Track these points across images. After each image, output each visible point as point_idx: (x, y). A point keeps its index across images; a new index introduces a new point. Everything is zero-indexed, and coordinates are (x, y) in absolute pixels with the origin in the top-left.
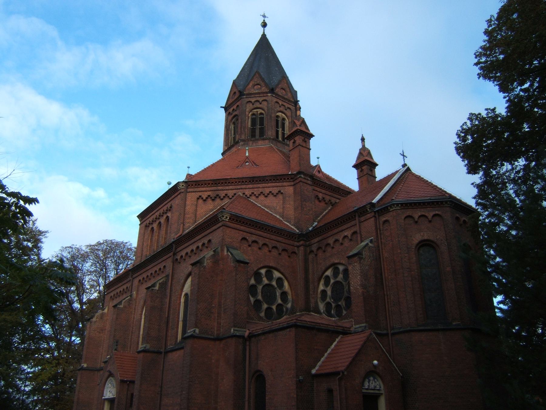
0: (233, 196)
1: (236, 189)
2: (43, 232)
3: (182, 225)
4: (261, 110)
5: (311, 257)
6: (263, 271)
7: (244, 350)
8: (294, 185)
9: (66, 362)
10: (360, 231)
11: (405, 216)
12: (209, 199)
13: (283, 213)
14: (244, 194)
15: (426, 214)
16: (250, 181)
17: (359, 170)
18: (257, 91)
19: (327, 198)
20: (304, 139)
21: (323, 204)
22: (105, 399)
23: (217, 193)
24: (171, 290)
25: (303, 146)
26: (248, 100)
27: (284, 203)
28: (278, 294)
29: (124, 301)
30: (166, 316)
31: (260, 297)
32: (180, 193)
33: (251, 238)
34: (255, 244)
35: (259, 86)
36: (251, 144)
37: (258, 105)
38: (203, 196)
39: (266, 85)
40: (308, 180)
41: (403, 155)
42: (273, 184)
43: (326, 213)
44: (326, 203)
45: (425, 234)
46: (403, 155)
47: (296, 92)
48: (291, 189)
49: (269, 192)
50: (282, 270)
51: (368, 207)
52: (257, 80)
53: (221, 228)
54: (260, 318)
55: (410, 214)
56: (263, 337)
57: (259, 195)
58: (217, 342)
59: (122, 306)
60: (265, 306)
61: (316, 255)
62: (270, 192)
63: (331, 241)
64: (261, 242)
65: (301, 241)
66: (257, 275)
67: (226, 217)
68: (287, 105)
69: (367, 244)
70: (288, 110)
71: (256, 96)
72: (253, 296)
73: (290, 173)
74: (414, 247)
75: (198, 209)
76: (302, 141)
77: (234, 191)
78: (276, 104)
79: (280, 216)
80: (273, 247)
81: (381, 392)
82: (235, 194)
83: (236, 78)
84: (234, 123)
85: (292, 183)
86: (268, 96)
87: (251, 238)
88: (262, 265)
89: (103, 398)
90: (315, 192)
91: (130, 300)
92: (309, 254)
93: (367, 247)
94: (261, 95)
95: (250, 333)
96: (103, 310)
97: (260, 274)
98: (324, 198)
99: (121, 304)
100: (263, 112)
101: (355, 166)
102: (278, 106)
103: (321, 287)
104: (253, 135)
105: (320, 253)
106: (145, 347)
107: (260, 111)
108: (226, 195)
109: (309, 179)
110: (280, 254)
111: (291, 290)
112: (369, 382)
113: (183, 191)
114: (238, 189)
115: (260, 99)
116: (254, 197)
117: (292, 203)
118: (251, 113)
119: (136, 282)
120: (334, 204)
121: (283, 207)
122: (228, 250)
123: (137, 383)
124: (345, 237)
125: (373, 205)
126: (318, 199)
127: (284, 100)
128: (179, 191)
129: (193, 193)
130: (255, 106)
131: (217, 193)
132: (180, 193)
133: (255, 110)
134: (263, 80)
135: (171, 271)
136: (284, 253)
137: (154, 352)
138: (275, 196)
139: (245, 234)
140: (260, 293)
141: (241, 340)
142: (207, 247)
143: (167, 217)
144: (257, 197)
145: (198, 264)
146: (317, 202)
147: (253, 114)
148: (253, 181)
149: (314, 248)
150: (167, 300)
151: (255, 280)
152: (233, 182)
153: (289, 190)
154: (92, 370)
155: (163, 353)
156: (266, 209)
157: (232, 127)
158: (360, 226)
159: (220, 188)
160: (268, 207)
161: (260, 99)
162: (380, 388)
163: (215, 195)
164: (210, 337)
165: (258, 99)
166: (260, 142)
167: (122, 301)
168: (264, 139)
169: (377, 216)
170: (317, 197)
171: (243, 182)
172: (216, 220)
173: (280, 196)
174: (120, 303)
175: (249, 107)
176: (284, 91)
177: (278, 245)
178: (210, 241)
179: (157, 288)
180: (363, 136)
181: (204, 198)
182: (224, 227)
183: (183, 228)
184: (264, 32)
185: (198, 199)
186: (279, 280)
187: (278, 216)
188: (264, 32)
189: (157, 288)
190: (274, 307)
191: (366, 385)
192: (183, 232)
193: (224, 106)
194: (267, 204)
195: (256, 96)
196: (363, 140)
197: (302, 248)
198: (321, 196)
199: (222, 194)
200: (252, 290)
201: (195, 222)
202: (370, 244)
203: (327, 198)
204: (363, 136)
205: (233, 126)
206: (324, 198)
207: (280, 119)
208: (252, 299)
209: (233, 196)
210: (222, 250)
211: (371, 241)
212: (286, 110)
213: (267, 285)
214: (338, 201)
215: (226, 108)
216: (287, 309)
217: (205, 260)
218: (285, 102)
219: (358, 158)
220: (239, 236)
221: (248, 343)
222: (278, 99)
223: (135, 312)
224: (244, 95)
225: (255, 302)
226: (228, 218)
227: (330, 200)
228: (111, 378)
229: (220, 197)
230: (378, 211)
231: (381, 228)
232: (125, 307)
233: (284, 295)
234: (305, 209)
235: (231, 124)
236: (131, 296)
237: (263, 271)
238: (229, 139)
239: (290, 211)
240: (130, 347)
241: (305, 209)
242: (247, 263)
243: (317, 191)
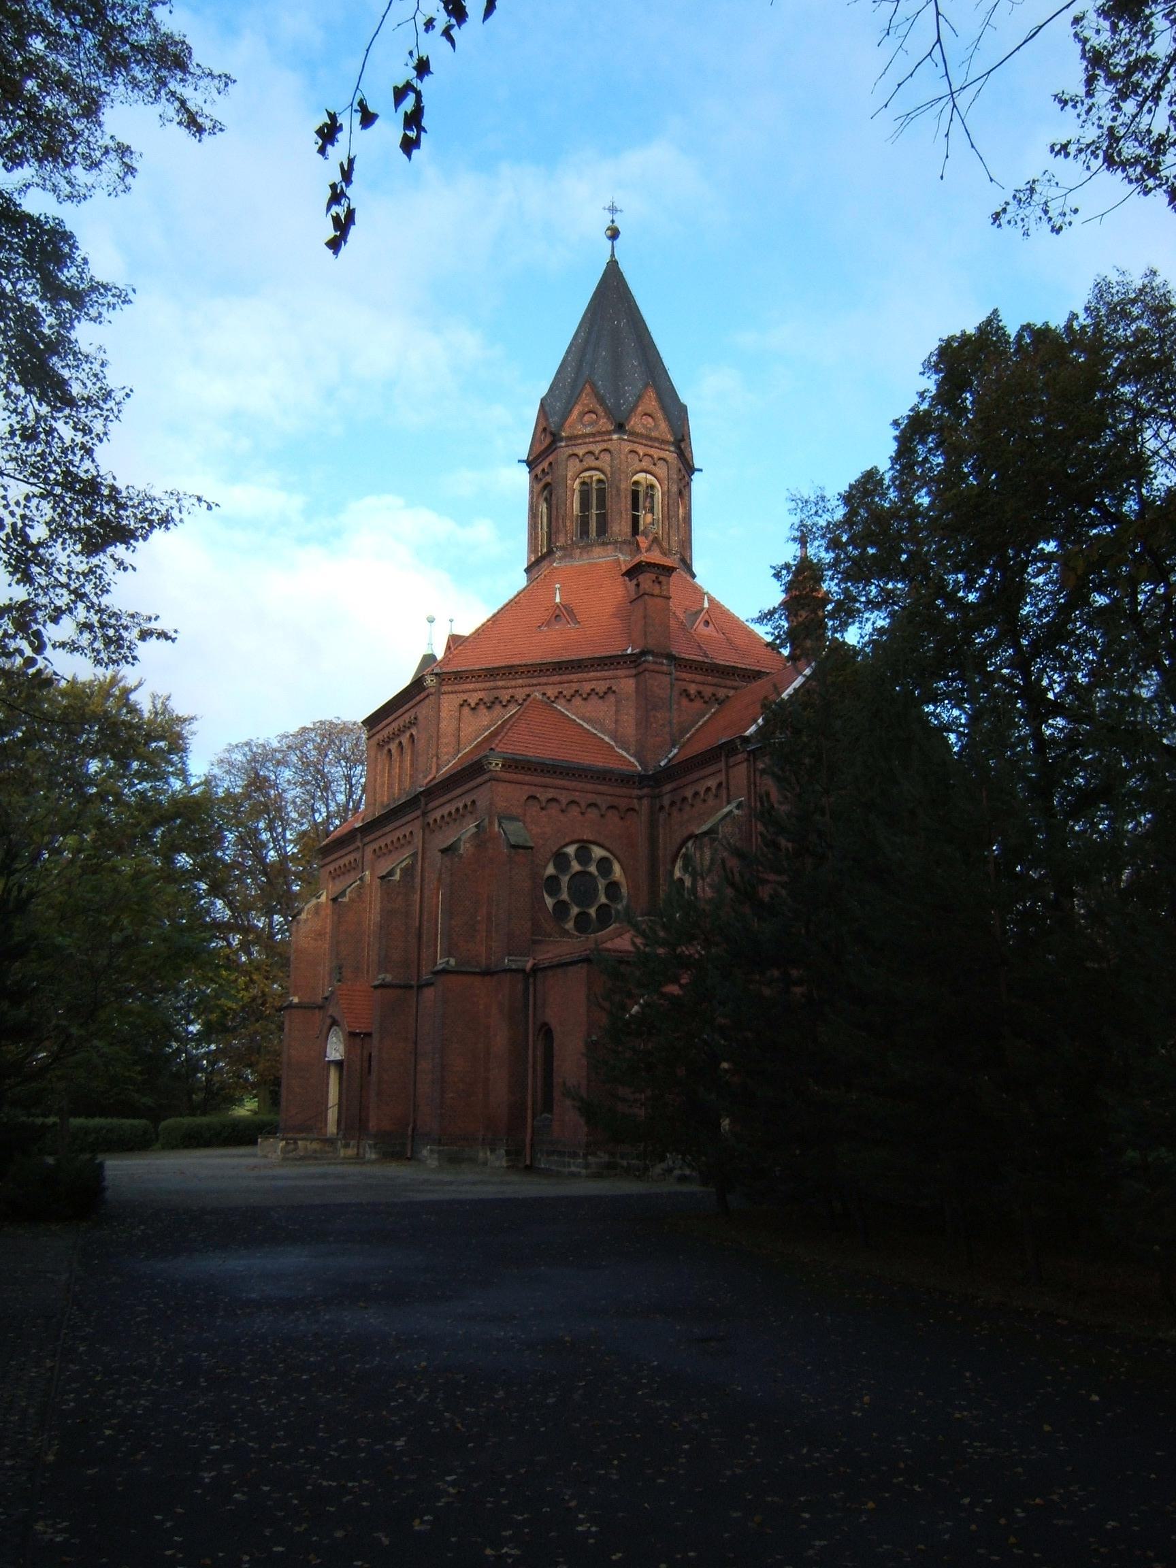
0: (524, 700)
1: (529, 686)
2: (185, 720)
3: (434, 760)
4: (597, 473)
5: (662, 816)
6: (571, 850)
7: (526, 989)
8: (635, 676)
9: (267, 978)
10: (728, 783)
12: (482, 706)
13: (616, 732)
14: (544, 694)
16: (554, 669)
18: (588, 430)
19: (708, 691)
21: (698, 704)
22: (329, 1061)
23: (496, 693)
24: (422, 880)
25: (652, 595)
26: (571, 452)
27: (617, 711)
28: (600, 887)
29: (349, 890)
30: (417, 924)
31: (565, 896)
32: (428, 696)
33: (544, 795)
34: (554, 804)
35: (594, 416)
36: (577, 556)
37: (590, 462)
38: (470, 701)
39: (609, 413)
40: (662, 664)
42: (598, 674)
43: (705, 723)
44: (705, 702)
47: (683, 409)
48: (632, 682)
50: (607, 845)
51: (738, 742)
52: (587, 400)
53: (489, 784)
54: (566, 933)
56: (550, 973)
57: (572, 696)
58: (487, 978)
59: (346, 899)
60: (575, 910)
61: (669, 814)
62: (593, 690)
63: (689, 793)
64: (564, 798)
65: (643, 787)
66: (561, 860)
67: (496, 764)
68: (656, 453)
69: (731, 812)
70: (661, 463)
71: (587, 440)
72: (551, 895)
73: (629, 651)
75: (462, 725)
76: (651, 584)
77: (527, 690)
78: (632, 455)
79: (611, 738)
80: (590, 805)
82: (528, 696)
83: (546, 391)
84: (546, 499)
85: (633, 672)
86: (611, 440)
87: (544, 795)
88: (567, 840)
90: (680, 683)
91: (360, 887)
93: (728, 819)
94: (597, 439)
95: (534, 965)
96: (319, 897)
97: (566, 855)
98: (699, 693)
99: (345, 896)
100: (602, 477)
102: (637, 458)
104: (585, 532)
105: (675, 813)
106: (383, 980)
107: (597, 475)
108: (512, 697)
110: (602, 816)
111: (626, 877)
113: (433, 690)
114: (533, 685)
115: (597, 448)
116: (562, 701)
117: (632, 711)
118: (578, 481)
119: (369, 851)
120: (723, 701)
121: (617, 721)
122: (500, 825)
123: (376, 1036)
124: (708, 789)
125: (746, 740)
126: (688, 695)
127: (650, 443)
128: (427, 691)
129: (451, 696)
130: (585, 464)
131: (496, 693)
132: (428, 696)
133: (587, 474)
134: (601, 400)
135: (420, 844)
136: (610, 813)
137: (400, 987)
138: (602, 698)
139: (534, 788)
140: (566, 890)
141: (520, 976)
142: (471, 813)
143: (412, 735)
144: (569, 700)
145: (450, 852)
146: (685, 701)
147: (583, 483)
148: (560, 669)
149: (666, 801)
150: (417, 897)
151: (556, 866)
152: (522, 672)
153: (627, 685)
154: (308, 1008)
155: (415, 988)
156: (585, 725)
157: (543, 507)
158: (727, 774)
159: (500, 683)
160: (588, 721)
161: (597, 448)
163: (492, 699)
164: (473, 970)
165: (592, 447)
166: (597, 551)
167: (345, 890)
168: (604, 544)
169: (751, 759)
170: (685, 693)
171: (541, 671)
173: (611, 698)
174: (343, 894)
175: (573, 466)
176: (650, 420)
177: (599, 800)
178: (473, 802)
179: (397, 877)
181: (473, 705)
182: (494, 782)
183: (438, 765)
184: (613, 255)
185: (461, 705)
186: (604, 865)
187: (607, 739)
188: (613, 255)
189: (397, 877)
190: (592, 911)
192: (437, 772)
194: (587, 714)
195: (587, 440)
197: (645, 802)
198: (692, 689)
199: (505, 697)
200: (552, 885)
201: (459, 751)
202: (736, 812)
203: (708, 691)
205: (545, 505)
206: (699, 693)
207: (641, 489)
208: (549, 902)
209: (524, 700)
210: (491, 823)
211: (739, 807)
212: (655, 464)
213: (578, 873)
214: (731, 693)
215: (531, 463)
216: (618, 912)
217: (462, 843)
218: (651, 447)
220: (522, 793)
221: (531, 980)
222: (635, 442)
223: (371, 908)
224: (561, 440)
225: (555, 905)
227: (714, 695)
228: (335, 1027)
229: (501, 702)
230: (753, 751)
231: (758, 781)
232: (352, 900)
233: (613, 888)
234: (654, 725)
235: (541, 501)
236: (361, 879)
237: (571, 850)
238: (536, 538)
239: (629, 729)
240: (368, 971)
241: (654, 725)
242: (531, 848)
243: (685, 680)
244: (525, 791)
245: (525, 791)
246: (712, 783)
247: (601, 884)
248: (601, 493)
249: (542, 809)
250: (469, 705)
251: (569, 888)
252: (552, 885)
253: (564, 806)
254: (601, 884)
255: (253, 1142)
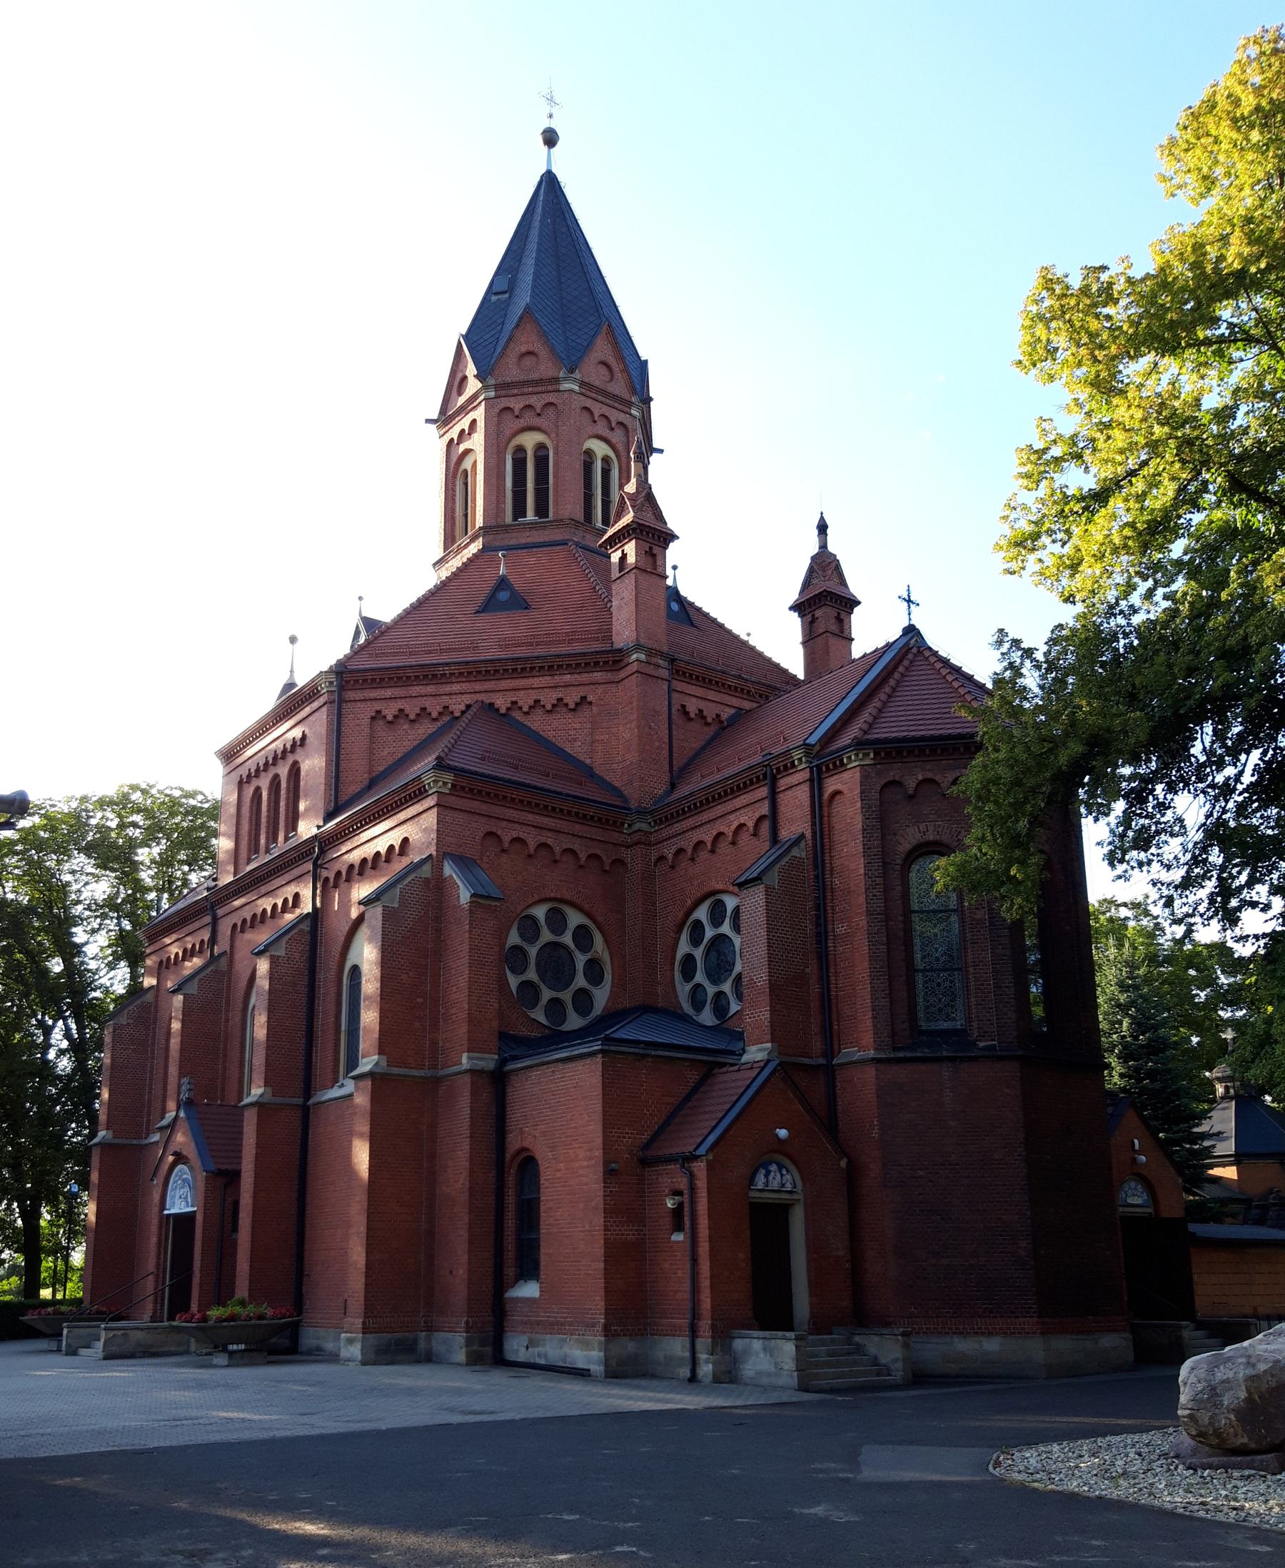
0: (463, 712)
6: (540, 912)
11: (883, 781)
15: (938, 778)
17: (806, 618)
20: (651, 548)
41: (909, 601)
45: (931, 829)
46: (909, 601)
49: (555, 702)
50: (586, 907)
55: (897, 778)
64: (532, 840)
71: (526, 390)
74: (899, 862)
81: (796, 1197)
89: (166, 1212)
92: (656, 865)
97: (533, 919)
101: (796, 607)
103: (684, 947)
109: (661, 662)
112: (767, 1176)
115: (538, 402)
126: (686, 713)
162: (795, 1187)
172: (419, 789)
173: (586, 712)
180: (822, 519)
185: (373, 718)
186: (582, 935)
191: (760, 1181)
193: (435, 417)
195: (526, 390)
196: (822, 528)
204: (822, 519)
219: (807, 584)
226: (450, 785)
237: (540, 912)
244: (481, 826)
245: (481, 826)
246: (748, 818)
247: (581, 960)
248: (542, 462)
249: (504, 851)
250: (385, 717)
251: (537, 964)
252: (516, 958)
253: (532, 852)
254: (581, 960)
255: (528, 1164)
